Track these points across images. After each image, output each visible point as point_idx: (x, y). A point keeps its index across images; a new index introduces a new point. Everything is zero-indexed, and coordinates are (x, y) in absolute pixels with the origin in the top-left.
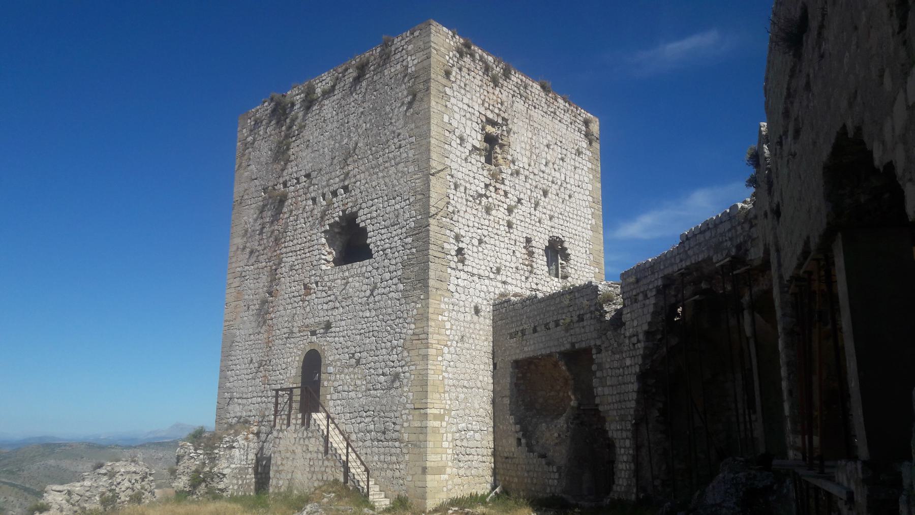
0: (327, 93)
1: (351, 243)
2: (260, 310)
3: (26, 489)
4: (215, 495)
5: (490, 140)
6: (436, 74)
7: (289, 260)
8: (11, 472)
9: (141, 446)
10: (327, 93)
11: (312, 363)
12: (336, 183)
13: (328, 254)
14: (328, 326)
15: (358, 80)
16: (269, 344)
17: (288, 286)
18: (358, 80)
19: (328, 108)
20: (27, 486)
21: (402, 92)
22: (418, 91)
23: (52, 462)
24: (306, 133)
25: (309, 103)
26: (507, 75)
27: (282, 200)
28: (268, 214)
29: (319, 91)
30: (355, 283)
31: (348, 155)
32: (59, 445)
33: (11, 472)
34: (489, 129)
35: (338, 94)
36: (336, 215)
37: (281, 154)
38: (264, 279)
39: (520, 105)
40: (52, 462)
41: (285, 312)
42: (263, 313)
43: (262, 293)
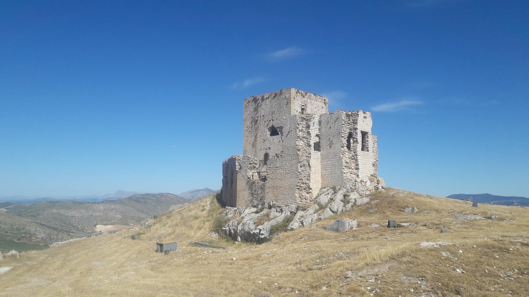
0: (267, 98)
1: (274, 132)
2: (488, 246)
3: (43, 225)
4: (319, 142)
5: (303, 109)
6: (292, 99)
7: (260, 134)
8: (34, 216)
9: (102, 202)
10: (267, 98)
11: (266, 156)
12: (270, 118)
13: (269, 133)
14: (270, 148)
15: (275, 97)
16: (256, 152)
17: (259, 140)
18: (275, 97)
19: (268, 101)
20: (43, 223)
21: (285, 101)
22: (288, 103)
23: (55, 211)
24: (262, 106)
25: (263, 99)
26: (306, 94)
27: (257, 121)
28: (253, 123)
29: (265, 97)
30: (275, 140)
31: (273, 113)
32: (57, 202)
33: (34, 216)
34: (303, 107)
35: (270, 99)
36: (271, 126)
37: (256, 110)
38: (253, 138)
39: (309, 100)
40: (55, 211)
41: (259, 145)
42: (254, 145)
43: (253, 141)
